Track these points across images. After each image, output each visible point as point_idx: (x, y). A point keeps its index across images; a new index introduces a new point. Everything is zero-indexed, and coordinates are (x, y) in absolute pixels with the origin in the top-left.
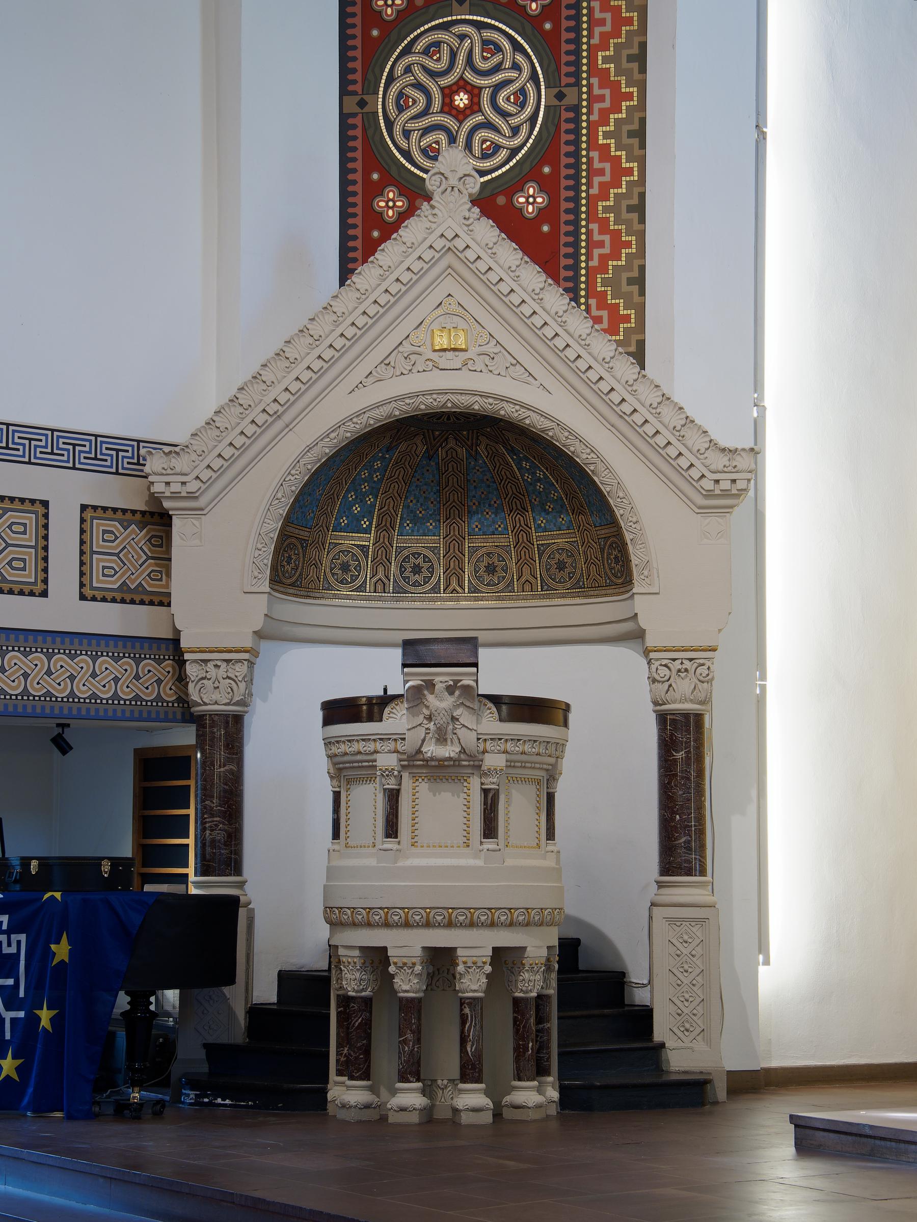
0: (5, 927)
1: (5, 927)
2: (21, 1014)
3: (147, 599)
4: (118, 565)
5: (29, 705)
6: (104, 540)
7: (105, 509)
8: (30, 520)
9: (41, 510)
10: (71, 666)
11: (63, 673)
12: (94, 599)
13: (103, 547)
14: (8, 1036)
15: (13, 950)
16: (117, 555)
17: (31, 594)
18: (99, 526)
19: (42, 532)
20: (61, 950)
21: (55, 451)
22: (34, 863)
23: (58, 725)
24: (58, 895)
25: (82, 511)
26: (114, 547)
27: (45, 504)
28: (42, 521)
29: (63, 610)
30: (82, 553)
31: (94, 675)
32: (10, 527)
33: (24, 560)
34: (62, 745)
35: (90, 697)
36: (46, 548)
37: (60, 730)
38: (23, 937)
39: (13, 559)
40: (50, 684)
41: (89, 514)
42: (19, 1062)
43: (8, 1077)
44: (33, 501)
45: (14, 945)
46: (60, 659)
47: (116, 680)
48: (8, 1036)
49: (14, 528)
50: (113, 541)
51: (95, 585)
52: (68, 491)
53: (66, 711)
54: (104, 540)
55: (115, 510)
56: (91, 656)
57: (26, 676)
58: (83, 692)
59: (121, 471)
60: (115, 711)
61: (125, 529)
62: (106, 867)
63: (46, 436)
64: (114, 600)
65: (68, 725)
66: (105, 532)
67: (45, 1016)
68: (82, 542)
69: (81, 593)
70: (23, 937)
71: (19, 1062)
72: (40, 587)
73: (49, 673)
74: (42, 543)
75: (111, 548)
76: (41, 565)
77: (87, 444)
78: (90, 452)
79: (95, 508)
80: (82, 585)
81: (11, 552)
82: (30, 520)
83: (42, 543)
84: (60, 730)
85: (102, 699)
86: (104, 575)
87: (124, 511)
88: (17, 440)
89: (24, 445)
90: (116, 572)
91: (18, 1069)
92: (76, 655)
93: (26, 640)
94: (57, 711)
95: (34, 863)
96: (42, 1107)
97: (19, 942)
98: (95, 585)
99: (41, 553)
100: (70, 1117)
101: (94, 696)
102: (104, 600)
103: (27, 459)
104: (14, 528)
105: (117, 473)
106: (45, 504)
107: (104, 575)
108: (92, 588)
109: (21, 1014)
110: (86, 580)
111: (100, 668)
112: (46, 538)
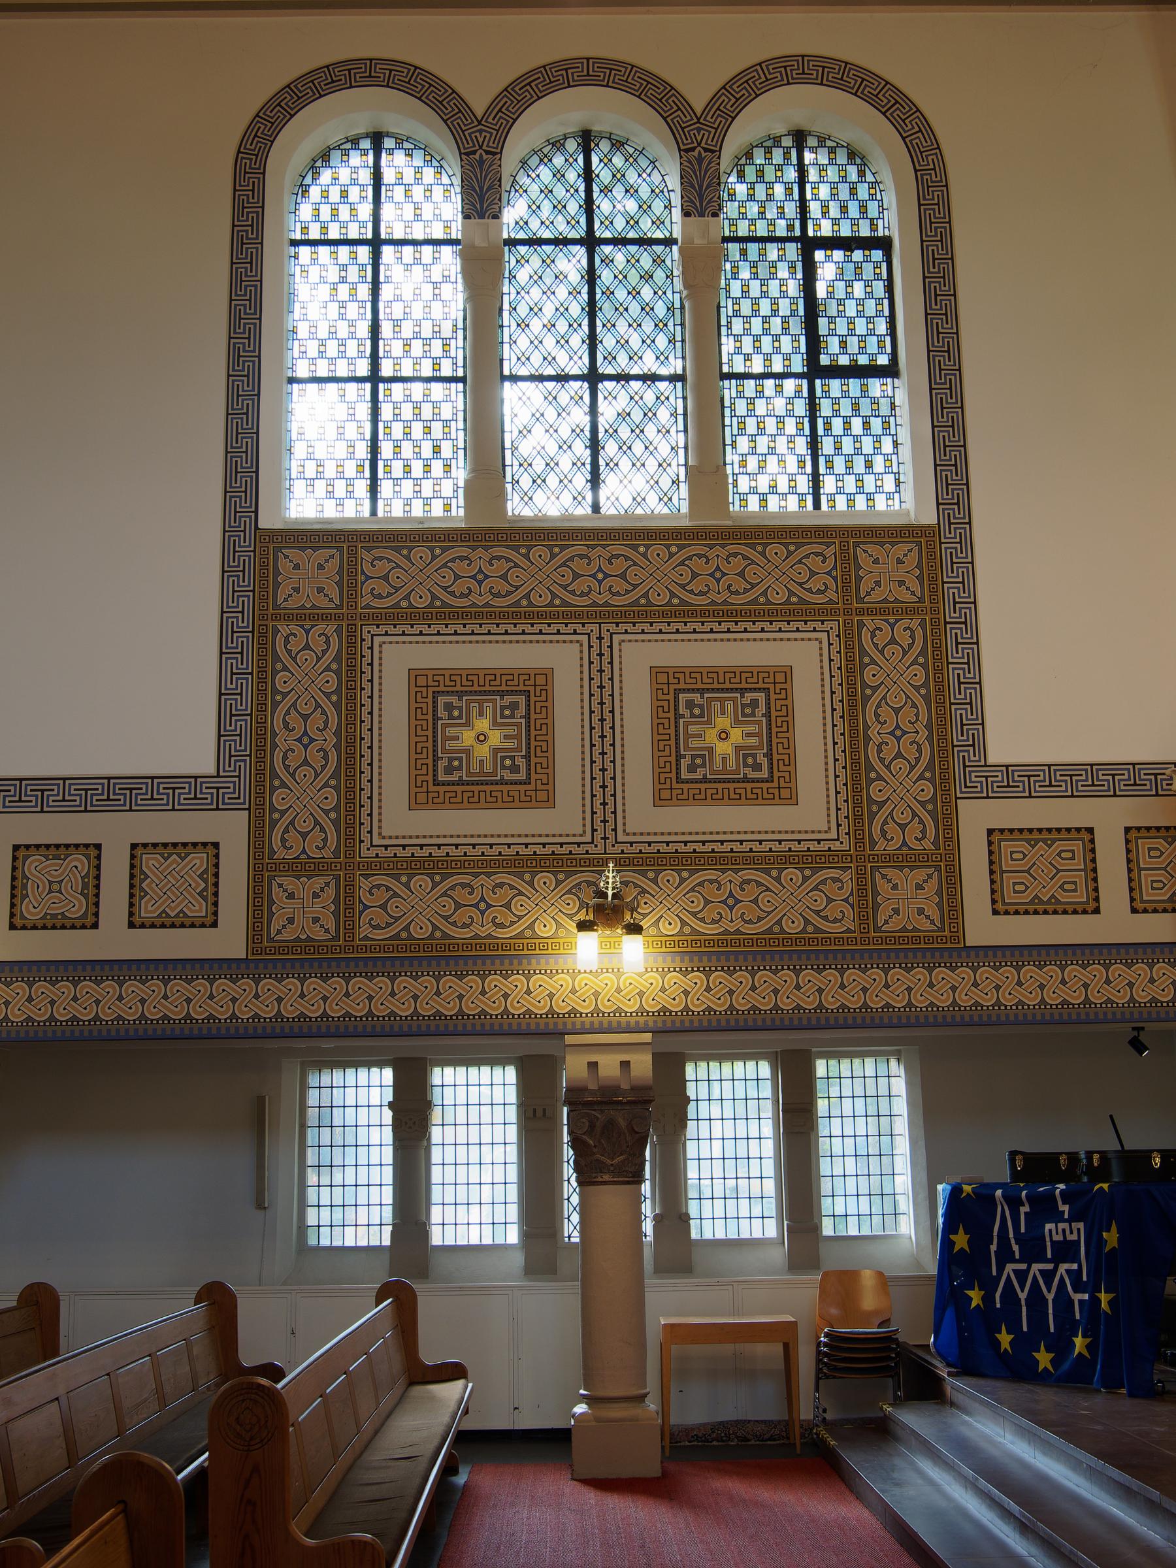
0: (1066, 1216)
1: (1066, 1216)
2: (1086, 1297)
3: (1060, 908)
4: (1166, 878)
5: (696, 1019)
6: (1150, 857)
7: (1148, 829)
8: (1077, 846)
9: (1087, 836)
10: (1129, 974)
11: (1121, 982)
12: (1145, 911)
13: (1150, 863)
14: (1078, 1317)
15: (1074, 1237)
16: (1165, 869)
17: (1085, 912)
18: (1144, 845)
19: (1089, 856)
20: (1111, 1237)
21: (1152, 777)
22: (1096, 1157)
23: (1134, 1029)
24: (1105, 1186)
25: (1126, 833)
26: (1161, 862)
27: (1090, 830)
28: (1089, 846)
29: (1117, 923)
30: (1130, 870)
31: (1152, 981)
32: (1059, 855)
33: (1075, 883)
34: (1137, 1045)
35: (1150, 1002)
36: (1095, 870)
37: (1136, 1033)
38: (1081, 1225)
39: (1065, 883)
40: (1110, 993)
41: (1133, 835)
42: (1089, 1340)
43: (1080, 1353)
44: (1078, 830)
45: (1075, 1232)
46: (1117, 969)
47: (909, 989)
48: (1078, 1317)
49: (1063, 855)
50: (1159, 857)
51: (1145, 898)
52: (1109, 817)
53: (1136, 1016)
54: (1150, 857)
55: (1158, 829)
56: (1147, 964)
57: (1086, 986)
58: (1142, 997)
59: (1160, 792)
60: (1132, 1014)
61: (200, 876)
62: (1157, 1161)
63: (1086, 770)
64: (1165, 911)
65: (1143, 1028)
66: (1150, 849)
67: (1104, 1298)
68: (1129, 861)
69: (1132, 907)
70: (1081, 1225)
71: (1089, 1340)
72: (1092, 905)
73: (1108, 982)
74: (1090, 866)
75: (1022, 866)
76: (1091, 885)
77: (999, 774)
78: (1129, 779)
79: (1138, 829)
80: (1132, 900)
81: (1062, 877)
82: (1077, 846)
83: (1090, 866)
84: (1136, 1033)
85: (1162, 1003)
86: (1153, 888)
87: (1167, 828)
88: (1058, 778)
89: (1066, 781)
90: (1165, 885)
91: (1088, 1347)
92: (1133, 964)
93: (1127, 953)
94: (1136, 1016)
95: (1096, 1157)
96: (1111, 1384)
97: (1079, 1230)
98: (1145, 898)
99: (1091, 875)
100: (1131, 1395)
101: (1154, 1000)
102: (1155, 911)
103: (1027, 794)
104: (1063, 855)
105: (1157, 795)
106: (1090, 830)
107: (1153, 888)
108: (1142, 901)
109: (1086, 1297)
110: (1136, 895)
111: (981, 978)
112: (1094, 860)
